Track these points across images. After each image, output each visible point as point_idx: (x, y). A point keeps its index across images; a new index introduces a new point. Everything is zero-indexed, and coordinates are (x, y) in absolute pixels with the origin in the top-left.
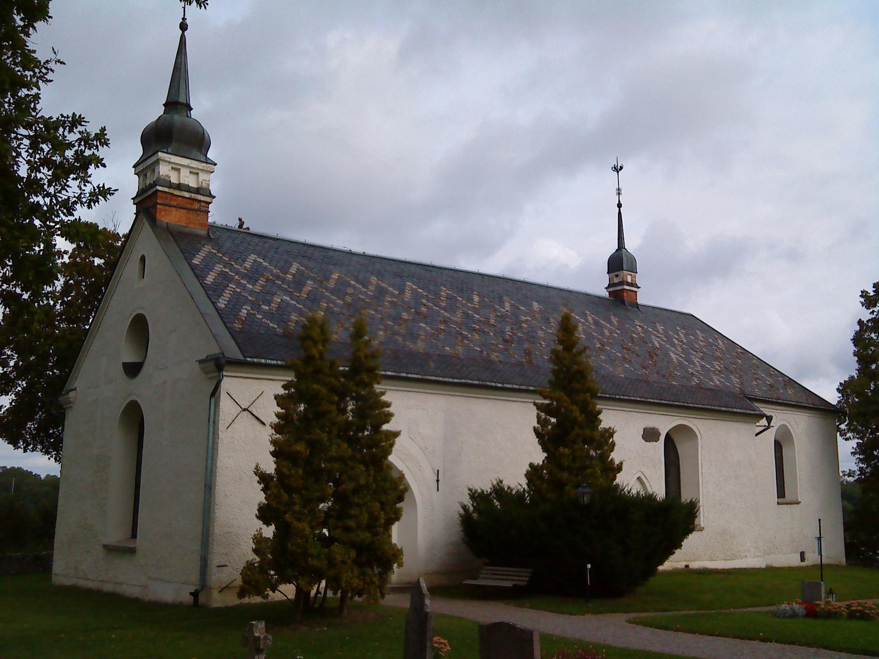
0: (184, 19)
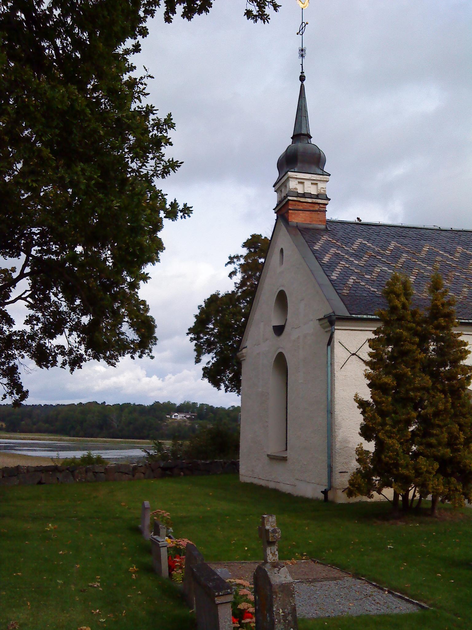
0: (302, 73)
